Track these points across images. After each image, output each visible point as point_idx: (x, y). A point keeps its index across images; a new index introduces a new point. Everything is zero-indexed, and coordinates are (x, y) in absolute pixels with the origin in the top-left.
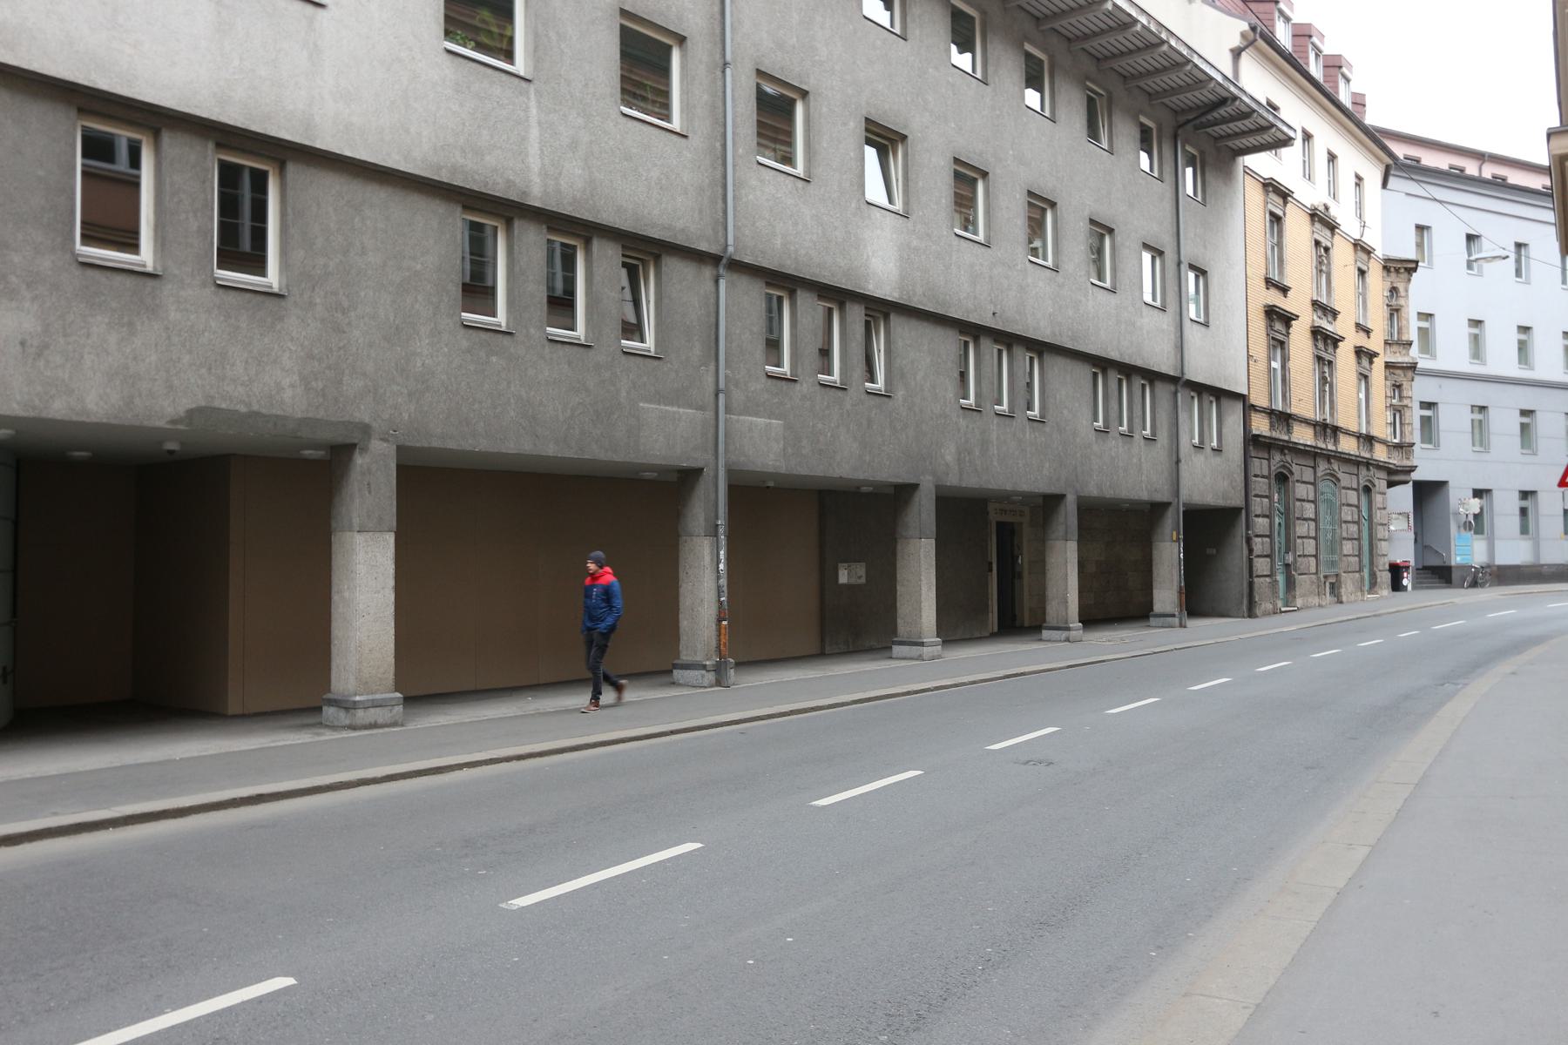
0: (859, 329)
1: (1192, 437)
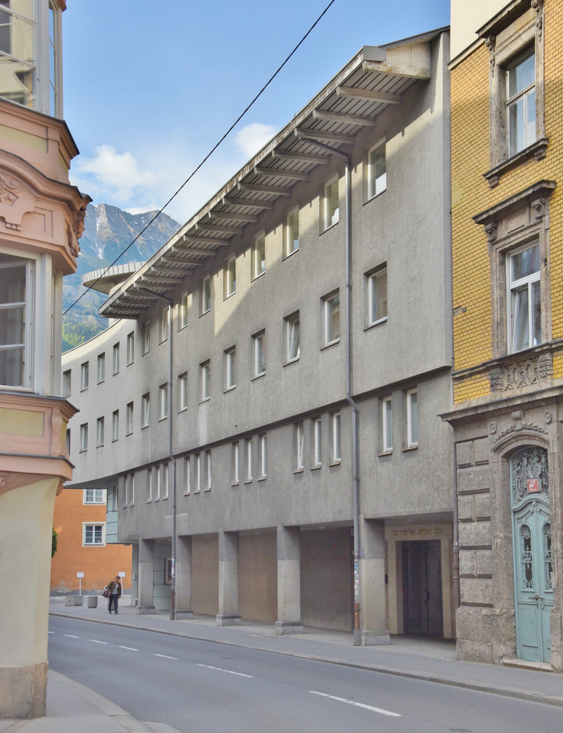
0: (242, 451)
1: (232, 477)
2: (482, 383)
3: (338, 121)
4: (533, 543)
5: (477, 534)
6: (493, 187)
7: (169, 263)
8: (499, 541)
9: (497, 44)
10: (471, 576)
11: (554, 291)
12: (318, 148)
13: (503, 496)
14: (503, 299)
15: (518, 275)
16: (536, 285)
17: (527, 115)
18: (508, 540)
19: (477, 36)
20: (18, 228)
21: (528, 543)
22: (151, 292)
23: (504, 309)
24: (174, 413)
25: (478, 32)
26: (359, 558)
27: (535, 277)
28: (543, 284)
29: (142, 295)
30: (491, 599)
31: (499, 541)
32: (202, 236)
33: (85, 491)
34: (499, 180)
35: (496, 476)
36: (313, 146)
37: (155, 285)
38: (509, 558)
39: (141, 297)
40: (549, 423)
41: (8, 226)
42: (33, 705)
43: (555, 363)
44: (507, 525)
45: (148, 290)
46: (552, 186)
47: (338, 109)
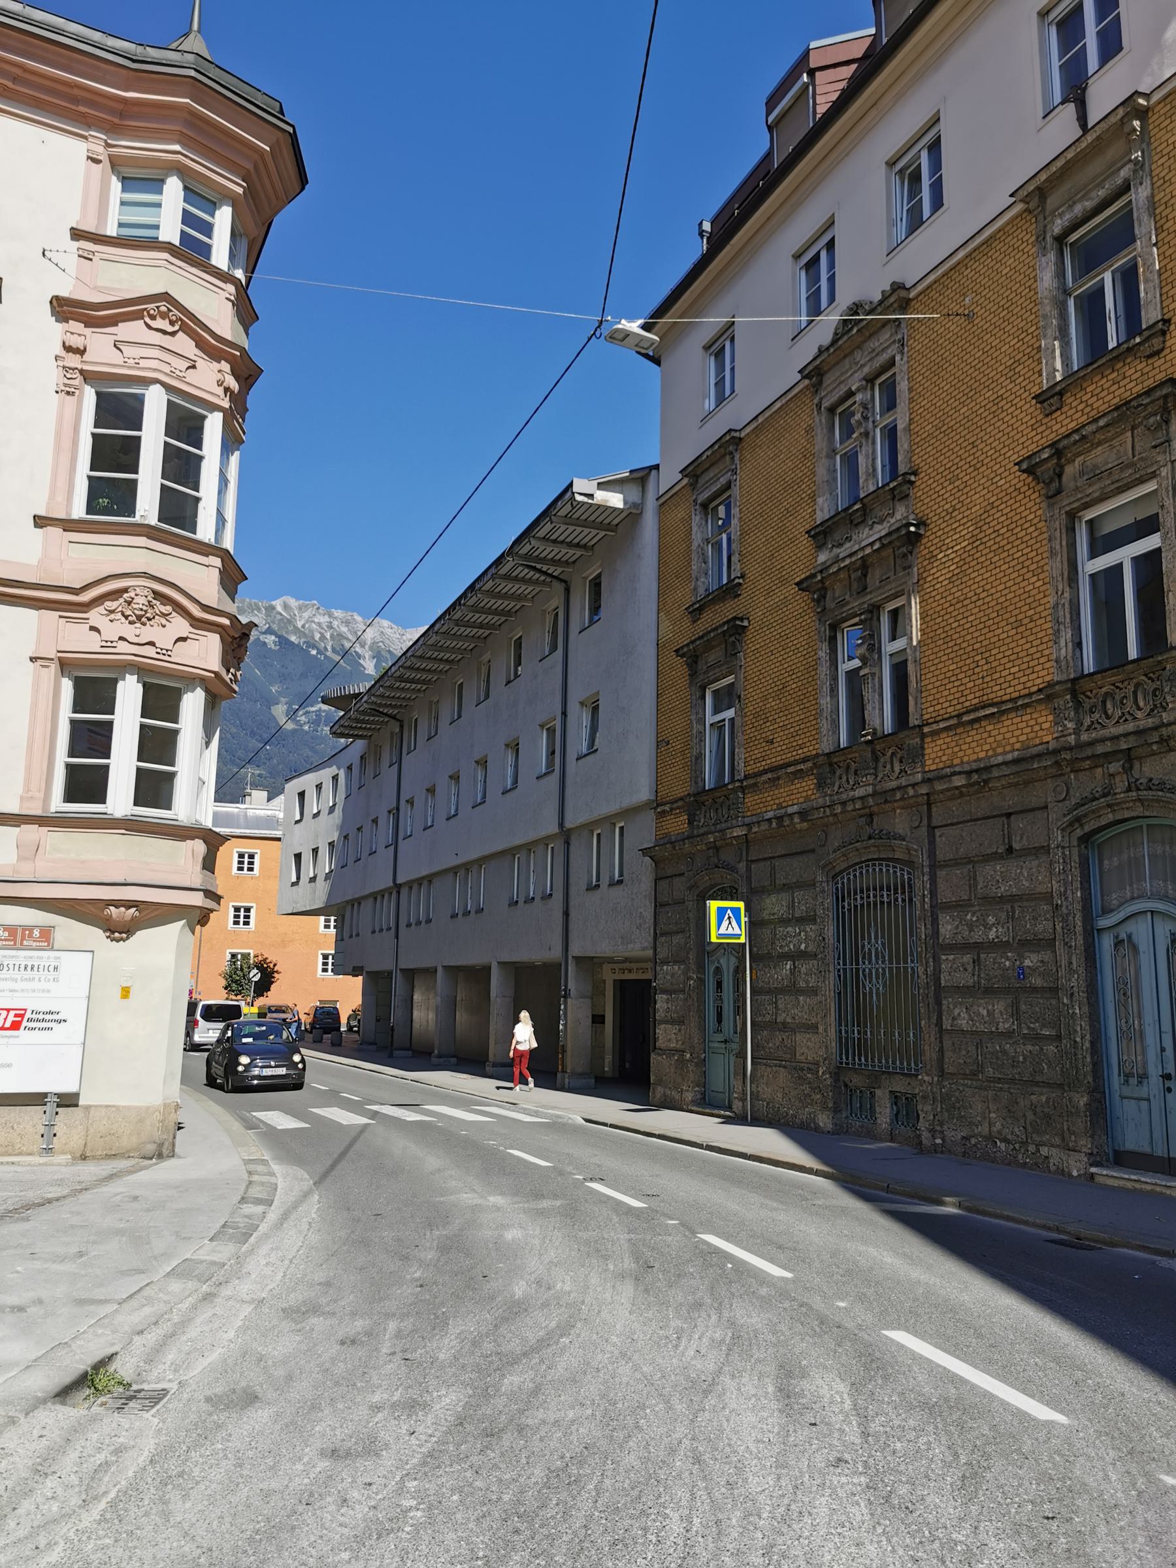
2: (681, 818)
3: (570, 551)
4: (725, 985)
5: (673, 975)
6: (694, 622)
7: (398, 684)
8: (692, 982)
9: (699, 485)
10: (666, 1022)
11: (747, 728)
12: (537, 575)
13: (697, 935)
14: (702, 734)
15: (717, 710)
16: (732, 720)
17: (591, 570)
18: (701, 981)
19: (680, 476)
20: (169, 653)
21: (719, 985)
22: (381, 713)
23: (703, 744)
24: (401, 836)
25: (681, 472)
26: (565, 997)
27: (730, 713)
28: (738, 722)
29: (373, 715)
30: (683, 1043)
31: (692, 982)
32: (429, 658)
33: (322, 918)
34: (700, 614)
35: (691, 915)
36: (532, 573)
37: (386, 705)
38: (701, 1001)
39: (372, 718)
40: (739, 862)
41: (159, 650)
42: (161, 1145)
43: (746, 800)
44: (701, 968)
45: (378, 711)
46: (746, 623)
47: (553, 537)
